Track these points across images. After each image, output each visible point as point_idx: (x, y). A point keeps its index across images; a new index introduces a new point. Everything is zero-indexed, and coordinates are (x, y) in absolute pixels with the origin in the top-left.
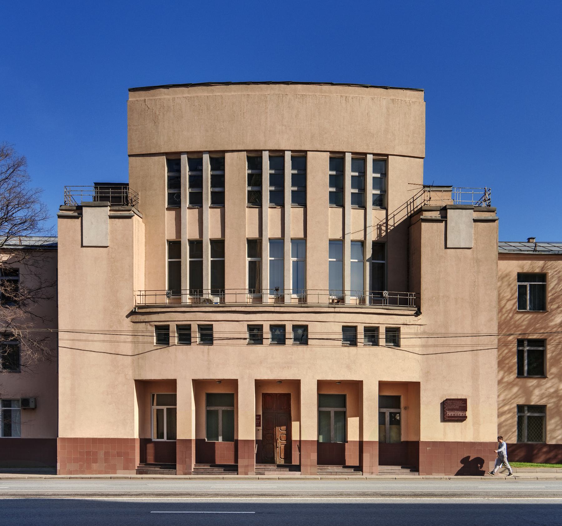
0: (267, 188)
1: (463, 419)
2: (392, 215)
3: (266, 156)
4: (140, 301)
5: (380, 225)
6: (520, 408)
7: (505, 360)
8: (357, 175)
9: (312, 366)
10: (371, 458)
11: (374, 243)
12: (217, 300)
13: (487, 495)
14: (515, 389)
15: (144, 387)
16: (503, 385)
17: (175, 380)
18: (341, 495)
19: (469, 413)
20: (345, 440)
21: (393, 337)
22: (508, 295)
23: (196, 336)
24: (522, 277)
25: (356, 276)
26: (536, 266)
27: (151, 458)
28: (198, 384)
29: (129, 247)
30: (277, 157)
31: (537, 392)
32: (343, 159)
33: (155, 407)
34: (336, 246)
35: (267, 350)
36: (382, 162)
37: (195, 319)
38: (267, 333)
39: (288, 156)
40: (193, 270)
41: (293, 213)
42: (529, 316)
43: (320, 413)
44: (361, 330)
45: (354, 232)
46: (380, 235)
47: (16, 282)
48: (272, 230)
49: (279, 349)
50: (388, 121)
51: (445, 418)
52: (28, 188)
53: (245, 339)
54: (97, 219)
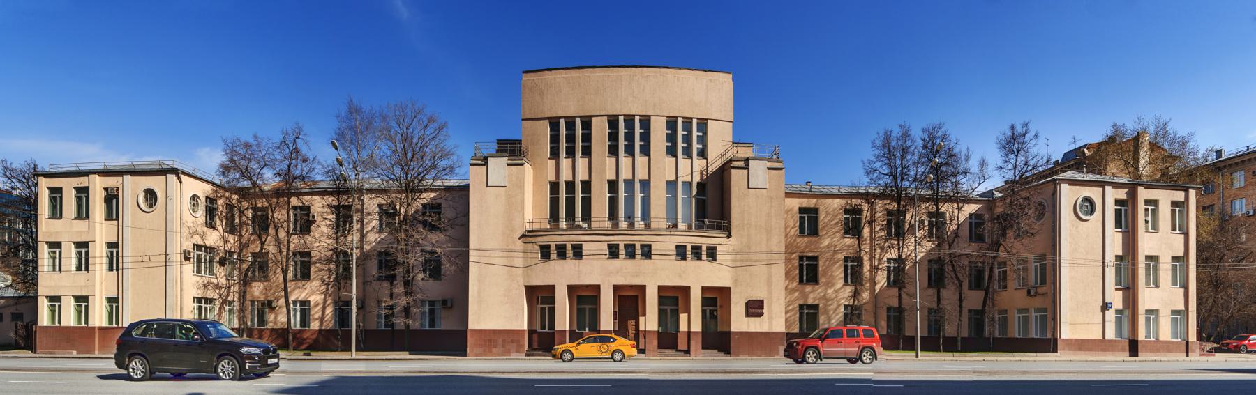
0: (622, 143)
1: (761, 315)
3: (621, 119)
4: (529, 227)
6: (801, 307)
8: (686, 134)
9: (655, 275)
10: (696, 344)
11: (699, 184)
12: (585, 225)
13: (776, 371)
14: (797, 294)
15: (531, 291)
17: (553, 287)
18: (673, 372)
19: (765, 311)
20: (678, 331)
21: (712, 253)
22: (791, 224)
23: (570, 252)
24: (802, 210)
25: (685, 208)
26: (812, 202)
27: (535, 345)
28: (571, 289)
29: (521, 186)
30: (629, 120)
31: (811, 296)
32: (676, 122)
33: (540, 306)
34: (672, 185)
35: (621, 262)
36: (703, 124)
37: (569, 240)
38: (622, 251)
39: (637, 119)
40: (568, 203)
41: (641, 161)
42: (806, 239)
43: (660, 310)
44: (689, 248)
45: (684, 176)
47: (439, 213)
48: (625, 174)
49: (630, 262)
50: (707, 94)
51: (748, 314)
52: (449, 144)
54: (498, 166)
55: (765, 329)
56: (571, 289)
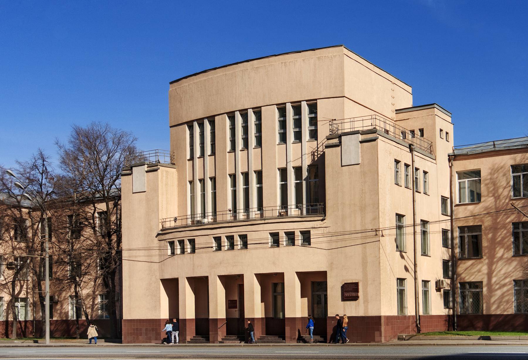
1: (356, 298)
2: (321, 144)
5: (314, 152)
7: (505, 239)
16: (504, 260)
19: (360, 294)
24: (515, 168)
35: (225, 254)
46: (313, 160)
51: (344, 299)
53: (267, 243)
55: (360, 313)
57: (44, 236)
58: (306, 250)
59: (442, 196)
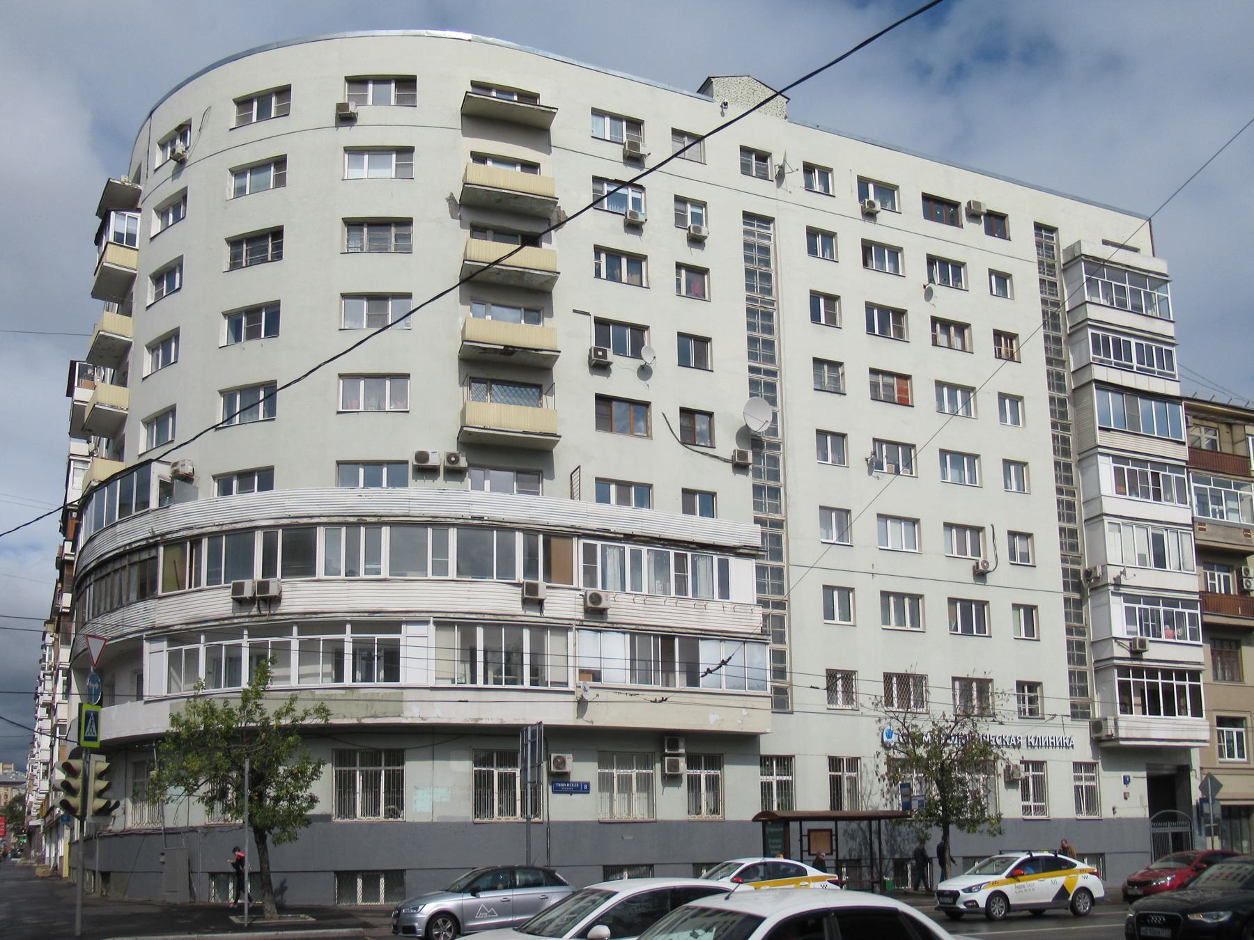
28: (608, 502)
56: (608, 502)
57: (476, 530)
58: (838, 470)
59: (1079, 242)
